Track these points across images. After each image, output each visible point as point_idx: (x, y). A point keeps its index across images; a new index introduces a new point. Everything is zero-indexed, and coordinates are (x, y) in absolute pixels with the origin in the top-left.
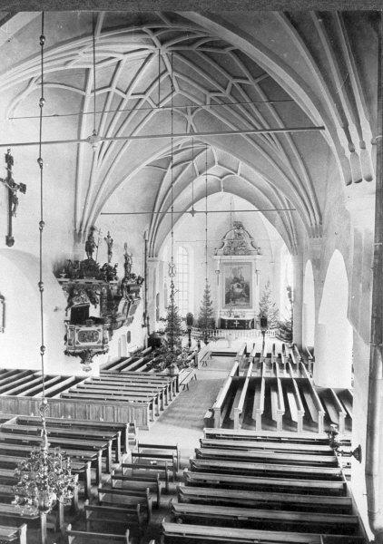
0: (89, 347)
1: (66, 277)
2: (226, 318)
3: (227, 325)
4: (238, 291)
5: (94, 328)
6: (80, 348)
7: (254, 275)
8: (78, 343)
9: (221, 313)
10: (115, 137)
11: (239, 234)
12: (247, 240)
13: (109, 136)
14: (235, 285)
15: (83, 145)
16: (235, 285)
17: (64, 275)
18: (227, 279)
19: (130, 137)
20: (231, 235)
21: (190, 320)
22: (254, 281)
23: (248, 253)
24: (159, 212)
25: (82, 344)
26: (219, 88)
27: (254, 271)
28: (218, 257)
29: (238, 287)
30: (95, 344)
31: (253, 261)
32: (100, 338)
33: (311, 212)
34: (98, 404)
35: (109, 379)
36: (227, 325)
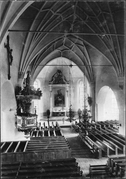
0: (31, 127)
1: (21, 94)
2: (55, 111)
3: (55, 114)
4: (60, 99)
5: (33, 118)
6: (27, 127)
7: (66, 93)
8: (26, 125)
9: (53, 110)
10: (42, 31)
11: (60, 75)
12: (63, 78)
13: (41, 30)
14: (58, 97)
15: (30, 33)
16: (58, 97)
17: (20, 94)
18: (55, 95)
19: (48, 32)
20: (56, 76)
21: (79, 113)
22: (66, 96)
23: (64, 83)
24: (35, 65)
25: (28, 125)
26: (95, 15)
27: (66, 91)
28: (51, 85)
29: (60, 98)
30: (33, 125)
31: (66, 87)
32: (35, 122)
33: (119, 66)
34: (30, 153)
35: (35, 141)
36: (55, 114)
